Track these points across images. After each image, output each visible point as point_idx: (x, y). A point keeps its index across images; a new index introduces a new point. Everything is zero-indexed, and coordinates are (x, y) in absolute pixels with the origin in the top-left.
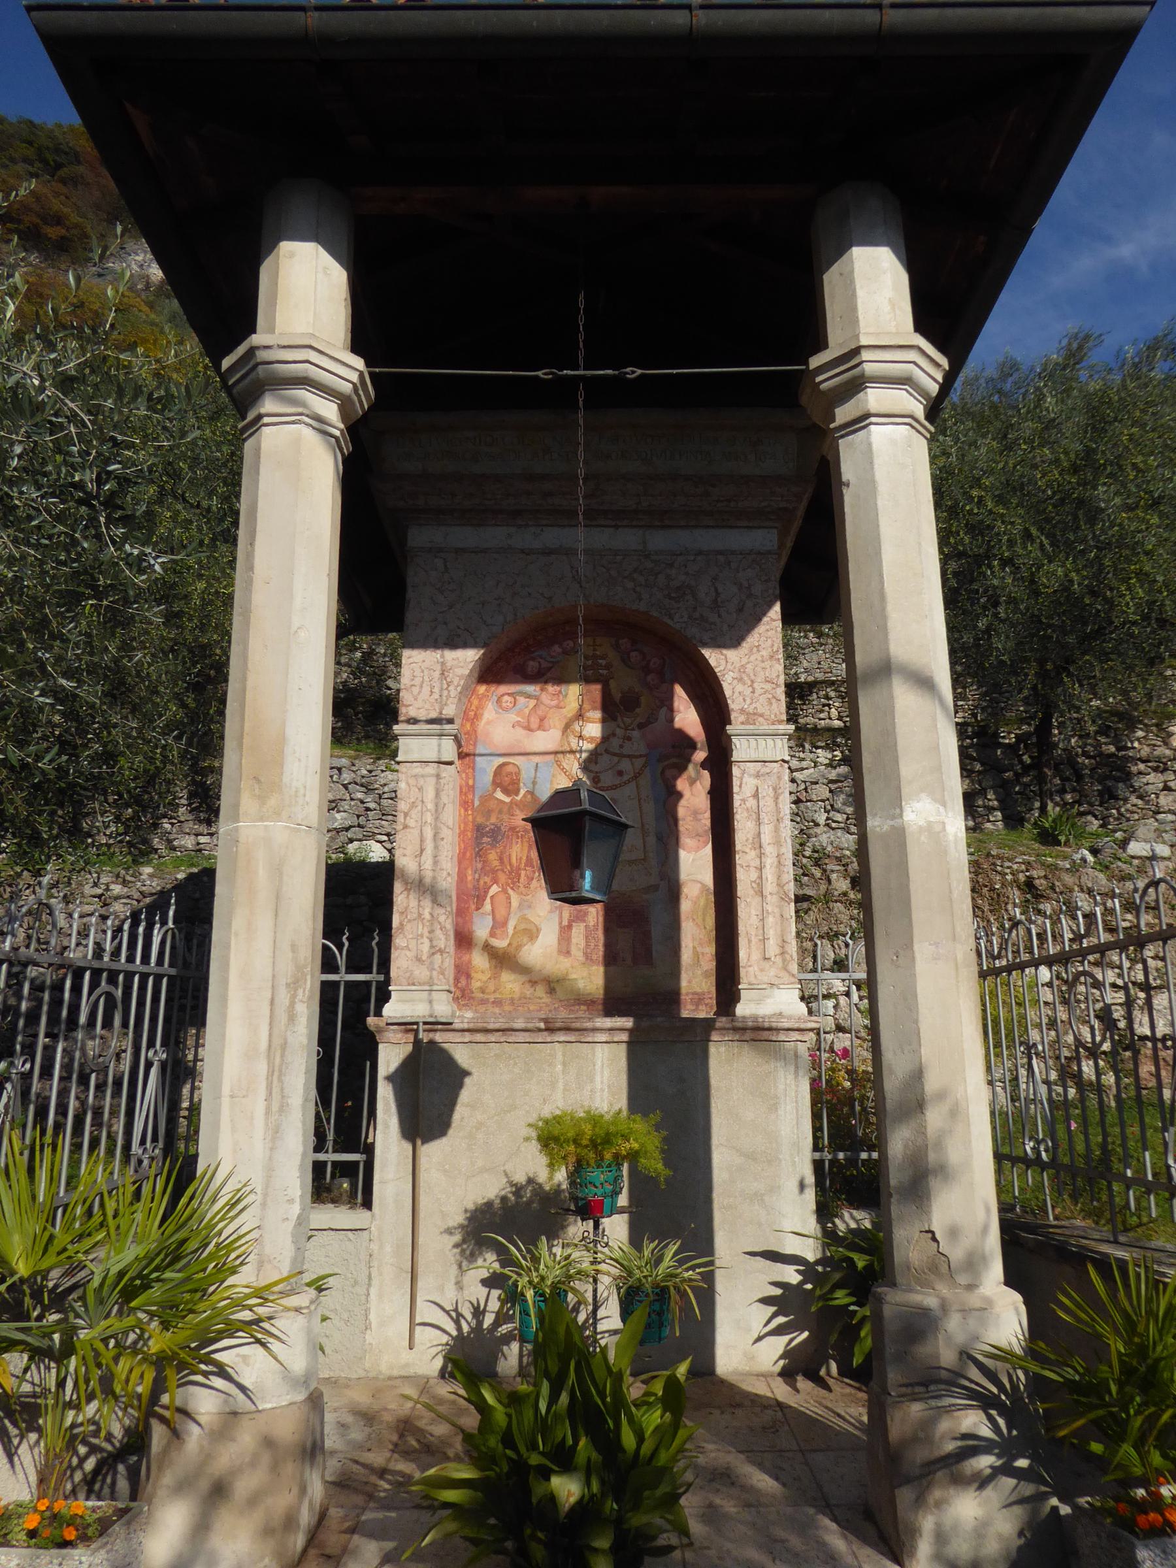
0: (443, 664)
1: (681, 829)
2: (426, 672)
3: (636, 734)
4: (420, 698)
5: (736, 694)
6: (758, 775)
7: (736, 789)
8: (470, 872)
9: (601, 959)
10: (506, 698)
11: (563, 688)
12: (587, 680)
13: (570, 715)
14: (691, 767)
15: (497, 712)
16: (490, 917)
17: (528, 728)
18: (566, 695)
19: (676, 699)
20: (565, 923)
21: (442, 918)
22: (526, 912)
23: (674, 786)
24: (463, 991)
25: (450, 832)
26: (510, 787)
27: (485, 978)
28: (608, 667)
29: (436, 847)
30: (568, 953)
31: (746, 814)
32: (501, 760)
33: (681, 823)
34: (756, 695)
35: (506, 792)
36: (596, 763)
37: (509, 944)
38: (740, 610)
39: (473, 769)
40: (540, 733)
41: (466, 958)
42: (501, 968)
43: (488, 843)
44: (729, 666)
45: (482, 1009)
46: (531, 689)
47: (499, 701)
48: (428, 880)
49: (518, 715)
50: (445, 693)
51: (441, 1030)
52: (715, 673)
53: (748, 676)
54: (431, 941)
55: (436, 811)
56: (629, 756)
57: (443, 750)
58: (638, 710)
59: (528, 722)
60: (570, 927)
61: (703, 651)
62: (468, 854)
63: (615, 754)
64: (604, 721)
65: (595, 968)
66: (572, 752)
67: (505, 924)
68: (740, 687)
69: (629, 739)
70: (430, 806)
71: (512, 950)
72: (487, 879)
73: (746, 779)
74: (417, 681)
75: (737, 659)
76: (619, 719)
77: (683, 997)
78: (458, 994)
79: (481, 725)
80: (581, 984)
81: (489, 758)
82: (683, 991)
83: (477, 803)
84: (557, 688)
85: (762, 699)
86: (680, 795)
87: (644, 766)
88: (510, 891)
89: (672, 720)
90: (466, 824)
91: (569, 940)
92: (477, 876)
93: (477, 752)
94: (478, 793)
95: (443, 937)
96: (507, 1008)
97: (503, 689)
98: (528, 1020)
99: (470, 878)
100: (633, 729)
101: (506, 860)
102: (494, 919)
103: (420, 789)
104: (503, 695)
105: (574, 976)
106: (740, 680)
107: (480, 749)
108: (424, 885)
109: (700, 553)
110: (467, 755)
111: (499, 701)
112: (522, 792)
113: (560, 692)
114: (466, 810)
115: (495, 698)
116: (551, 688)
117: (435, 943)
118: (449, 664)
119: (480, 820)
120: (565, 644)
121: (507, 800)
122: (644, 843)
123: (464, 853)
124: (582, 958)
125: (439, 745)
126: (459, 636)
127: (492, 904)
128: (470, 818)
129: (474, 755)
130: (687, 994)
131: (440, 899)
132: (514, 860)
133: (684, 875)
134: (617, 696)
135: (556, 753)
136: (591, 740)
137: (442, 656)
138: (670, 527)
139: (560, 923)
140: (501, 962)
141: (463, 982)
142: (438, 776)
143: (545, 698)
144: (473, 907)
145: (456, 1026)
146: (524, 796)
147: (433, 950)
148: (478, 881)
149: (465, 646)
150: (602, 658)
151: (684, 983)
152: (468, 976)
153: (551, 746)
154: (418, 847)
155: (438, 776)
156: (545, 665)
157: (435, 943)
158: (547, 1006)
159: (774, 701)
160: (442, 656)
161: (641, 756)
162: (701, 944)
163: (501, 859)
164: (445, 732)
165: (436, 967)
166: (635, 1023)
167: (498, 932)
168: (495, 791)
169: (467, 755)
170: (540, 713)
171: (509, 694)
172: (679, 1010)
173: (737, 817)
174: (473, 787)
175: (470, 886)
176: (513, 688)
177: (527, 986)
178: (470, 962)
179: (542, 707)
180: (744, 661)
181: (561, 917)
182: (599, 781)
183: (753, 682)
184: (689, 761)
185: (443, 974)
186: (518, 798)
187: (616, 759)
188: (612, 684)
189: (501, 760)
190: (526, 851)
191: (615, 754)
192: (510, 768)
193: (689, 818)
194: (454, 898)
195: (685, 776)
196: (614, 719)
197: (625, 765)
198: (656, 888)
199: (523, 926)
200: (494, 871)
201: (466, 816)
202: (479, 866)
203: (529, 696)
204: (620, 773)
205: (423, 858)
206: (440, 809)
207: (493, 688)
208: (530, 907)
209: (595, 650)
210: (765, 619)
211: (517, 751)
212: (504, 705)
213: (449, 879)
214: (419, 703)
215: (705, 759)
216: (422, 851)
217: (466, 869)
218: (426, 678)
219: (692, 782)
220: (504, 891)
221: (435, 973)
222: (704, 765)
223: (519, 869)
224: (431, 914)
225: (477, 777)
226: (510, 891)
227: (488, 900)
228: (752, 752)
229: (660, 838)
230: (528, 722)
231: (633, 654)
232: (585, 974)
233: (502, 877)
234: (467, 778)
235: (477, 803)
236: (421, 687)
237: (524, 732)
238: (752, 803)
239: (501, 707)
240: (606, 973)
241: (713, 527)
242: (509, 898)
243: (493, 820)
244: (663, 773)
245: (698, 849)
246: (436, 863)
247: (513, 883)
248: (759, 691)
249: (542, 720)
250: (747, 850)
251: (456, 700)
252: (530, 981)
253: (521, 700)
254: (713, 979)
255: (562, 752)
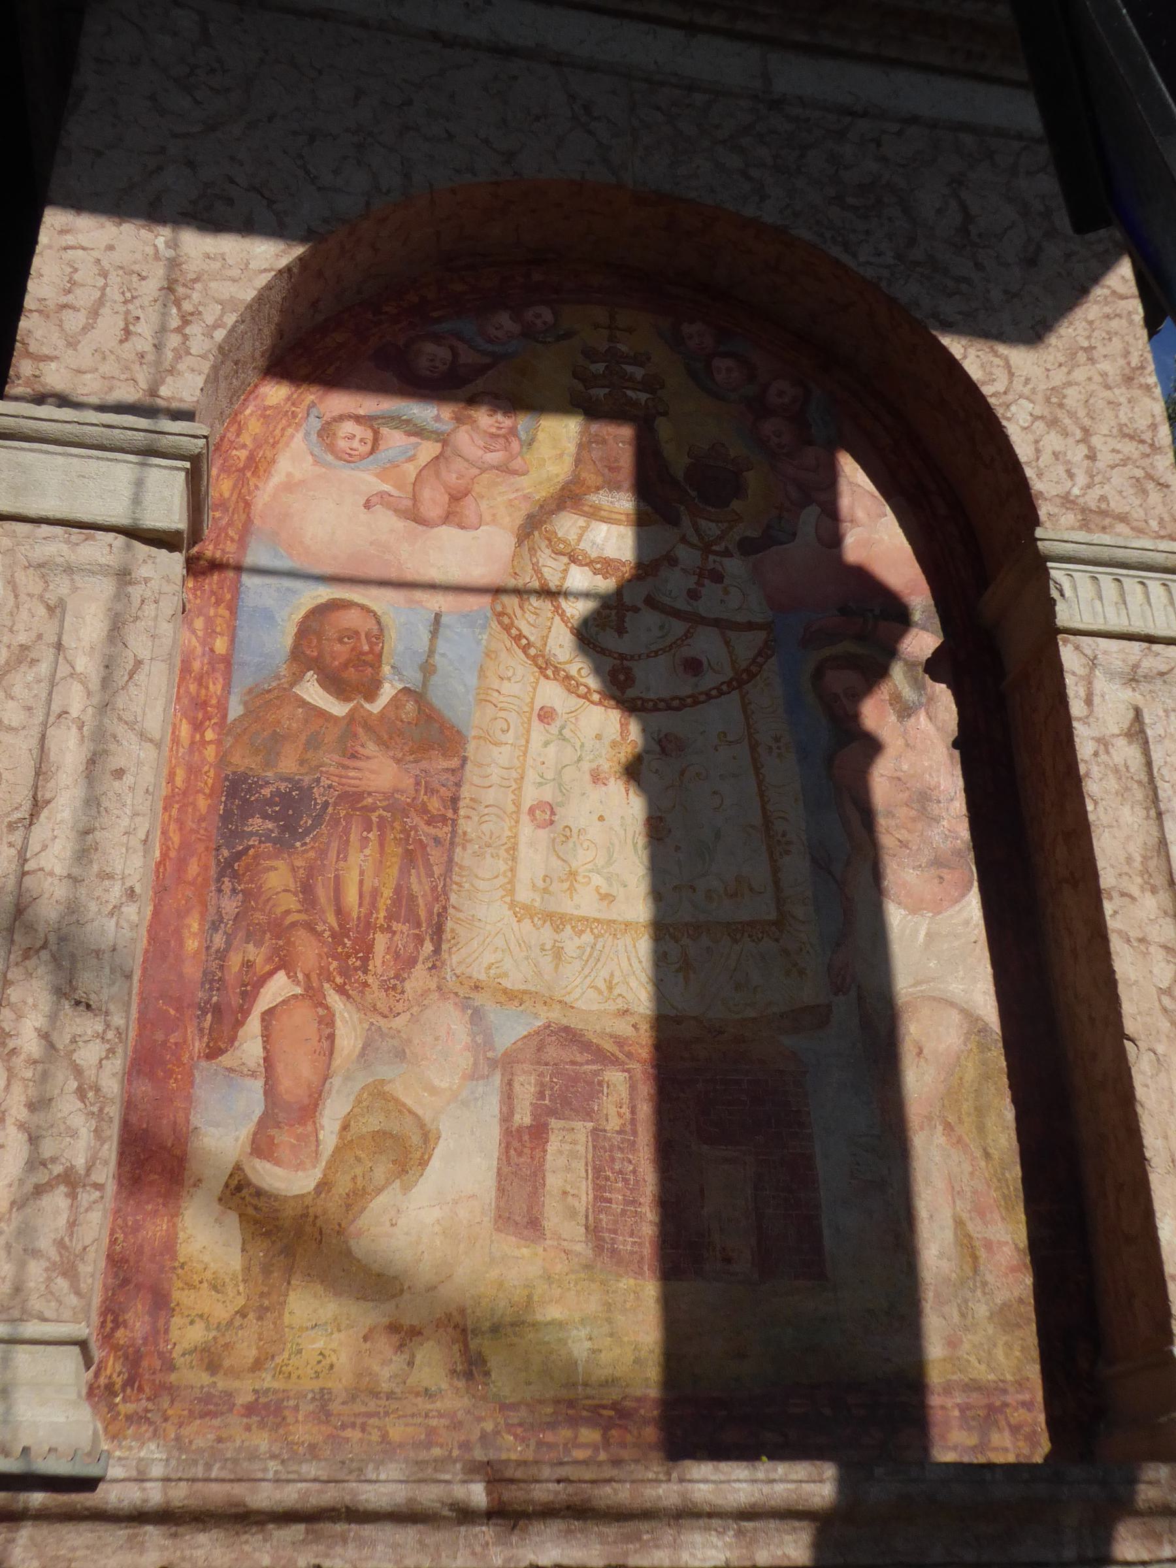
0: (174, 264)
1: (887, 840)
2: (114, 278)
3: (734, 566)
4: (86, 347)
5: (1046, 458)
6: (1133, 678)
7: (1077, 708)
8: (194, 924)
9: (647, 1251)
10: (349, 427)
11: (523, 422)
12: (591, 411)
13: (541, 494)
14: (898, 672)
15: (317, 462)
16: (258, 1085)
17: (415, 516)
18: (530, 443)
19: (844, 488)
20: (523, 1117)
21: (89, 1055)
22: (384, 1071)
23: (856, 717)
24: (133, 1359)
25: (148, 753)
26: (351, 674)
27: (222, 1312)
28: (651, 385)
29: (93, 802)
30: (533, 1226)
31: (1112, 784)
32: (324, 593)
33: (882, 822)
34: (1100, 465)
35: (335, 684)
36: (621, 631)
37: (323, 1186)
38: (1032, 262)
39: (233, 609)
40: (447, 533)
41: (155, 1229)
42: (289, 1271)
43: (266, 837)
44: (1018, 385)
45: (201, 1435)
46: (424, 412)
47: (327, 432)
48: (48, 911)
49: (382, 475)
50: (174, 340)
51: (43, 1516)
52: (981, 399)
53: (1072, 414)
54: (34, 1140)
55: (105, 682)
56: (717, 623)
57: (149, 498)
58: (736, 505)
59: (415, 498)
60: (538, 1133)
61: (946, 341)
62: (193, 869)
63: (677, 614)
64: (641, 521)
65: (626, 1283)
66: (549, 593)
67: (309, 1110)
68: (1052, 441)
69: (717, 577)
70: (86, 664)
71: (332, 1205)
72: (257, 954)
73: (1101, 684)
74: (84, 297)
75: (1037, 372)
76: (686, 521)
77: (935, 1400)
78: (114, 1369)
79: (265, 494)
80: (579, 1345)
81: (287, 583)
82: (936, 1376)
83: (235, 710)
84: (504, 421)
85: (1119, 478)
86: (873, 747)
87: (764, 653)
88: (335, 1000)
89: (836, 541)
90: (193, 771)
91: (536, 1177)
92: (219, 940)
93: (250, 560)
94: (243, 681)
95: (83, 1127)
96: (303, 1432)
97: (340, 402)
98: (421, 1472)
99: (192, 945)
100: (727, 553)
101: (323, 894)
102: (270, 1091)
103: (56, 609)
104: (341, 418)
105: (554, 1312)
106: (1053, 423)
107: (257, 555)
108: (30, 928)
109: (914, 120)
110: (216, 566)
111: (327, 432)
112: (388, 691)
113: (513, 431)
114: (198, 727)
115: (315, 424)
116: (485, 419)
117: (48, 1148)
118: (192, 267)
119: (242, 761)
120: (529, 315)
121: (338, 708)
122: (775, 871)
123: (181, 865)
124: (582, 1248)
125: (139, 484)
126: (230, 202)
127: (267, 1037)
128: (210, 752)
129: (239, 569)
130: (948, 1390)
131: (87, 981)
132: (351, 897)
133: (905, 983)
134: (678, 461)
135: (497, 591)
136: (604, 566)
137: (174, 244)
138: (834, 53)
139: (506, 1118)
140: (288, 1252)
141: (137, 1324)
142: (124, 576)
143: (463, 438)
144: (198, 1046)
145: (111, 1495)
146: (395, 702)
147: (42, 1177)
148: (222, 955)
149: (247, 227)
150: (636, 361)
151: (935, 1349)
152: (161, 1303)
153: (480, 572)
154: (23, 796)
155: (124, 576)
156: (468, 357)
157: (48, 1148)
158: (456, 1425)
159: (1150, 486)
160: (174, 244)
161: (750, 626)
162: (980, 1212)
163: (307, 890)
164: (165, 442)
165: (45, 1243)
166: (844, 1483)
167: (284, 1138)
168: (297, 679)
169: (216, 566)
170: (452, 478)
171: (358, 419)
172: (925, 1449)
173: (1091, 787)
174: (227, 661)
175: (192, 971)
176: (370, 404)
177: (384, 1344)
178: (169, 1246)
179: (458, 465)
180: (1058, 377)
181: (508, 1097)
182: (630, 680)
183: (1086, 431)
184: (891, 653)
185: (69, 1271)
186: (375, 707)
187: (678, 628)
188: (664, 429)
189: (324, 593)
190: (393, 871)
191: (677, 614)
192: (351, 619)
193: (902, 812)
194: (136, 977)
195: (883, 692)
196: (672, 520)
197: (707, 644)
198: (818, 1017)
199: (373, 1122)
200: (279, 929)
201: (197, 745)
202: (230, 906)
203: (418, 431)
204: (693, 666)
205: (40, 833)
206: (121, 676)
207: (311, 395)
208: (400, 1055)
209: (611, 339)
210: (1098, 292)
211: (374, 572)
212: (342, 444)
213: (131, 911)
214: (84, 356)
215: (937, 652)
216: (37, 805)
217: (182, 914)
218: (113, 293)
219: (905, 711)
220: (313, 995)
221: (36, 1270)
222: (935, 667)
223: (368, 925)
224: (45, 1036)
225: (242, 634)
226: (335, 1000)
227: (253, 1024)
228: (1111, 612)
229: (822, 863)
230: (415, 498)
231: (721, 364)
232: (593, 1305)
233: (308, 951)
234: (210, 632)
235: (235, 710)
236: (95, 313)
237: (400, 524)
238: (1126, 753)
239: (331, 448)
240: (669, 1305)
241: (941, 71)
242: (328, 1021)
243: (288, 764)
244: (818, 674)
245: (937, 907)
246: (85, 851)
247: (345, 972)
248: (1105, 458)
249: (457, 497)
250: (1135, 891)
251: (206, 366)
252: (394, 1328)
253: (395, 440)
254: (1029, 1334)
255: (517, 592)
